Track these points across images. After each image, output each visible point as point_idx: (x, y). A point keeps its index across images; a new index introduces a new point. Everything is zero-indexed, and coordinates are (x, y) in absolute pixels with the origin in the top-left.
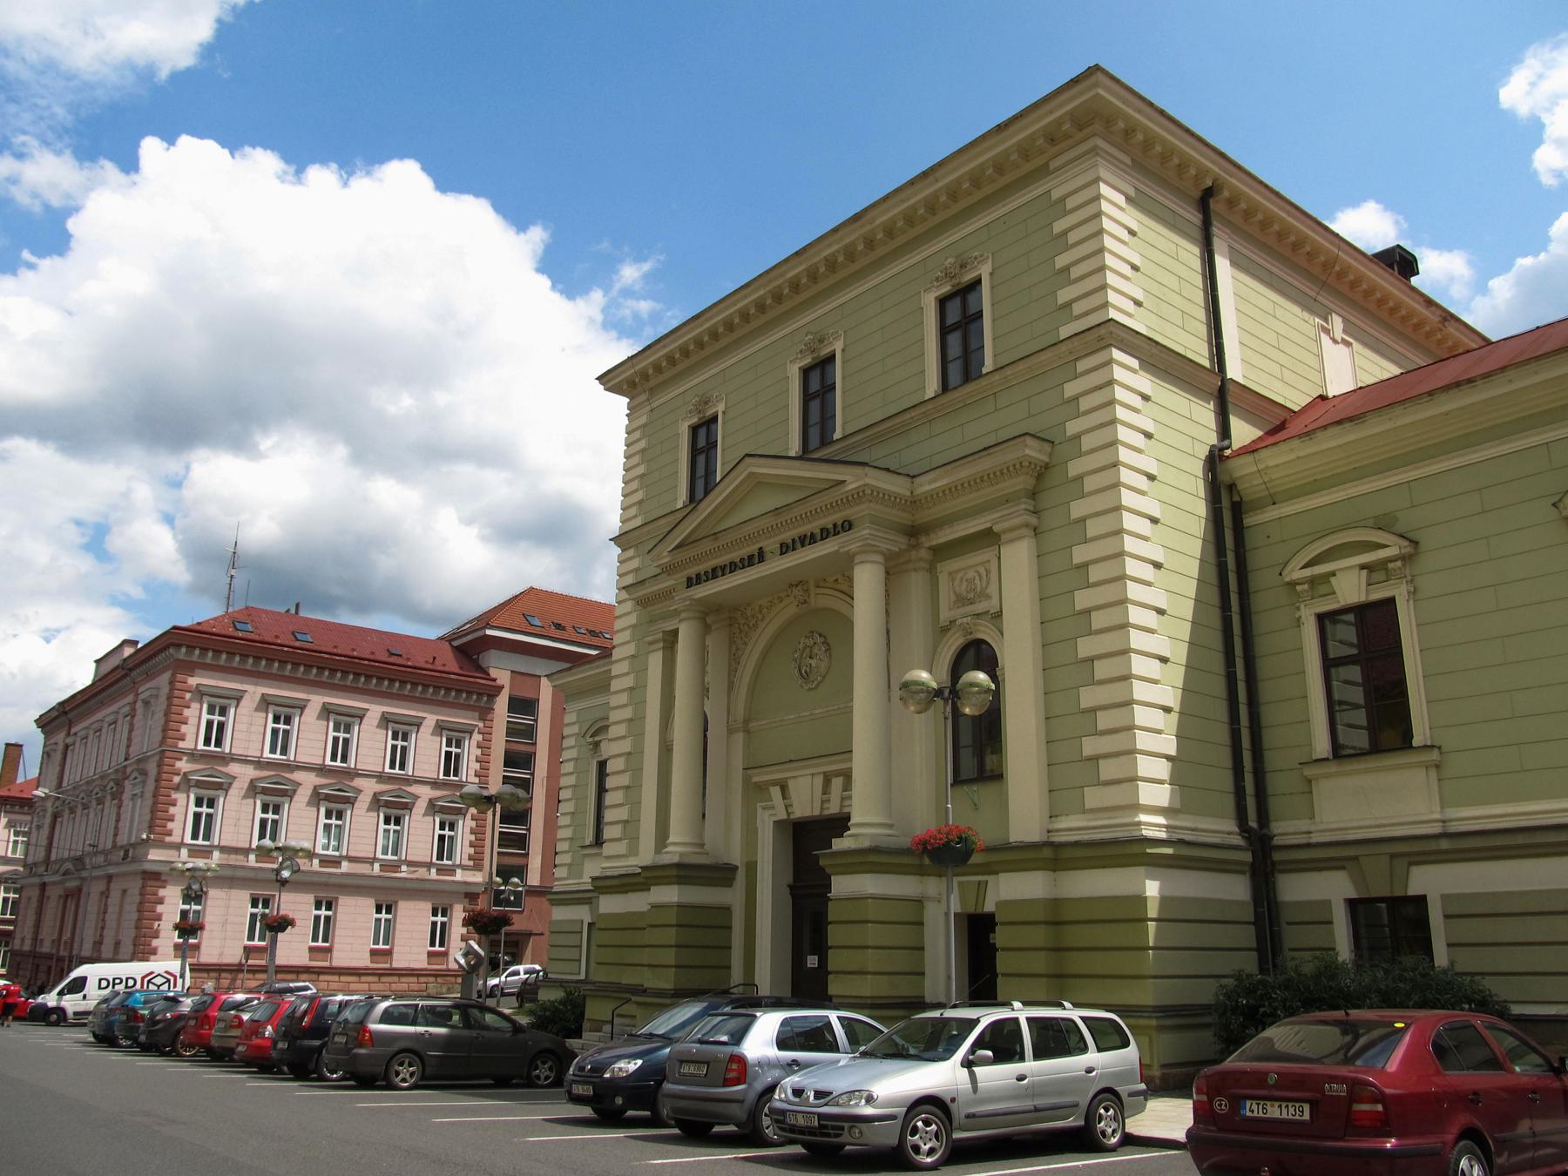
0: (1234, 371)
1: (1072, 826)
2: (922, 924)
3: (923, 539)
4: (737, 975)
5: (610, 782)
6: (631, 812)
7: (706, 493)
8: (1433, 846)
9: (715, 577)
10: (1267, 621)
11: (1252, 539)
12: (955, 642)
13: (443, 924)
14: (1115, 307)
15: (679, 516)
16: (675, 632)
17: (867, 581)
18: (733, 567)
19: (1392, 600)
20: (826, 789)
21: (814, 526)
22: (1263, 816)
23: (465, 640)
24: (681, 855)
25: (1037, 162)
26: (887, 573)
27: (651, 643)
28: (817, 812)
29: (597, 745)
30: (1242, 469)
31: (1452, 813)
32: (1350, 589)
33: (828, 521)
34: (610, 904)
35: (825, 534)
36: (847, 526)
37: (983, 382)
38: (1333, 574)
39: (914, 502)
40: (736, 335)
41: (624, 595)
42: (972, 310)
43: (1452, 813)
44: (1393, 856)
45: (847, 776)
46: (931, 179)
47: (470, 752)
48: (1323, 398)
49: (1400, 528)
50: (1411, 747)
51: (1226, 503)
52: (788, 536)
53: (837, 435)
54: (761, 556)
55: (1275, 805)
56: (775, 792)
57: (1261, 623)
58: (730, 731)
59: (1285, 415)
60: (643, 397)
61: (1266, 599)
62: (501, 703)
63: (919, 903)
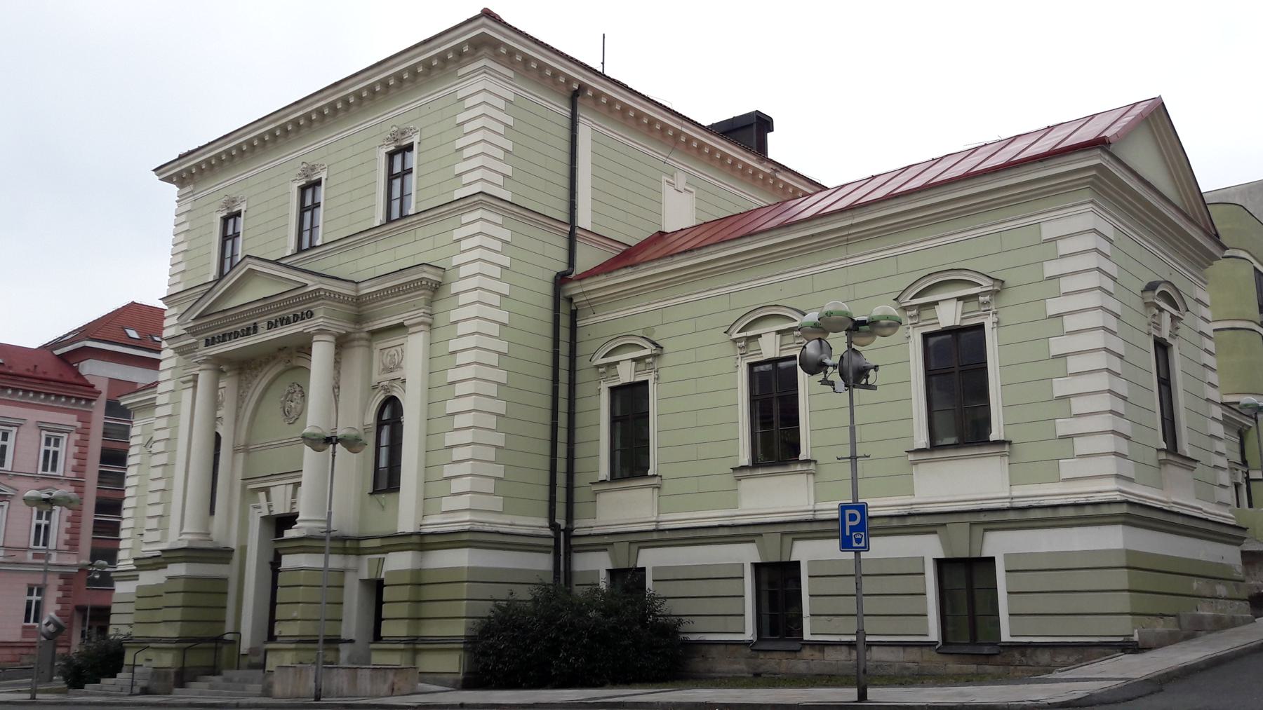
0: (584, 219)
4: (229, 627)
6: (165, 510)
7: (232, 268)
8: (648, 537)
11: (580, 335)
12: (380, 397)
15: (210, 286)
18: (236, 335)
19: (646, 382)
22: (570, 516)
24: (190, 541)
27: (184, 382)
32: (626, 374)
35: (297, 318)
36: (310, 315)
38: (618, 363)
42: (407, 167)
43: (663, 517)
48: (662, 234)
54: (254, 329)
55: (578, 509)
56: (262, 495)
57: (580, 391)
58: (236, 451)
63: (342, 572)
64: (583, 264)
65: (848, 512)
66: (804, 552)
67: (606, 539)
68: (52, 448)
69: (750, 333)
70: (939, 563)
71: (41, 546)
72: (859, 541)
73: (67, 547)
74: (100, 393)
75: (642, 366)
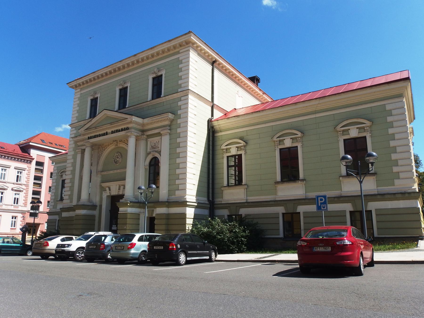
0: (215, 102)
1: (173, 198)
2: (139, 219)
3: (145, 133)
5: (66, 185)
9: (95, 137)
10: (218, 156)
13: (15, 221)
14: (191, 87)
16: (84, 150)
17: (132, 141)
18: (100, 136)
20: (119, 189)
21: (120, 128)
23: (23, 145)
25: (177, 50)
26: (136, 140)
28: (117, 194)
29: (62, 176)
30: (215, 124)
31: (249, 198)
33: (123, 127)
34: (64, 214)
35: (122, 130)
37: (161, 99)
39: (143, 125)
40: (103, 78)
41: (71, 139)
44: (237, 206)
45: (124, 186)
46: (153, 50)
47: (24, 175)
49: (244, 140)
50: (299, 180)
51: (211, 130)
52: (113, 129)
53: (127, 106)
54: (107, 134)
56: (107, 189)
59: (227, 112)
60: (79, 90)
61: (218, 152)
62: (34, 162)
64: (216, 117)
65: (319, 198)
66: (301, 209)
67: (227, 205)
68: (19, 175)
69: (281, 139)
70: (283, 214)
71: (16, 204)
72: (324, 207)
73: (24, 205)
74: (33, 159)
75: (295, 141)
